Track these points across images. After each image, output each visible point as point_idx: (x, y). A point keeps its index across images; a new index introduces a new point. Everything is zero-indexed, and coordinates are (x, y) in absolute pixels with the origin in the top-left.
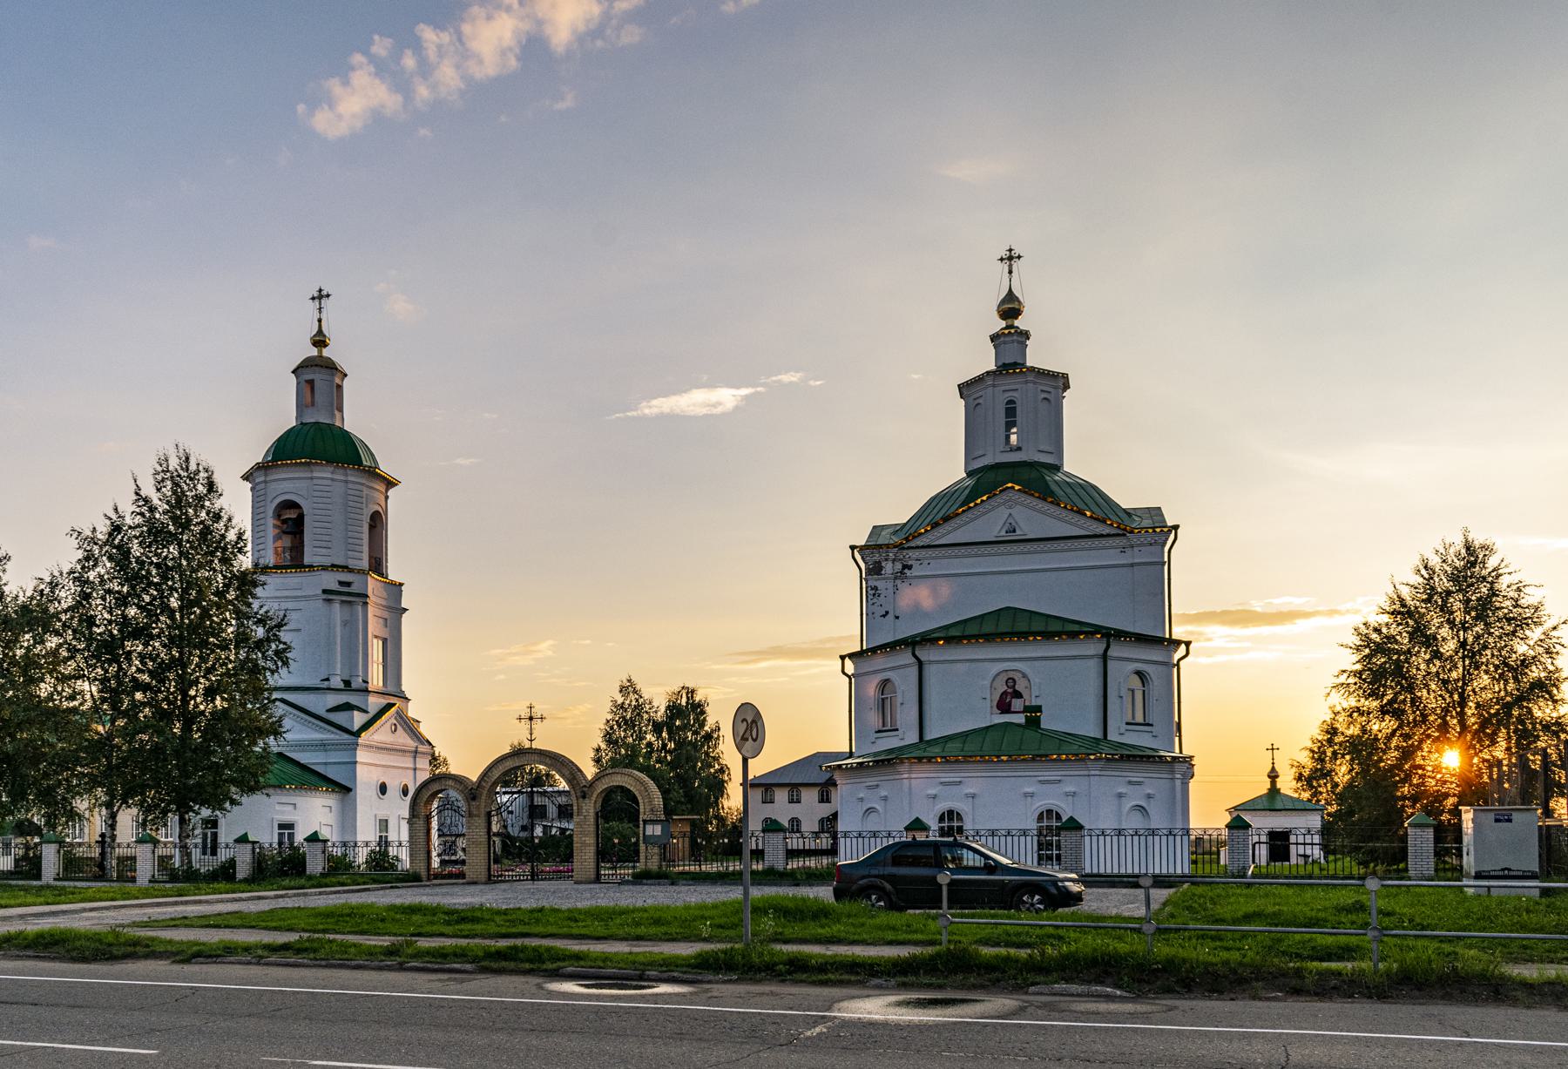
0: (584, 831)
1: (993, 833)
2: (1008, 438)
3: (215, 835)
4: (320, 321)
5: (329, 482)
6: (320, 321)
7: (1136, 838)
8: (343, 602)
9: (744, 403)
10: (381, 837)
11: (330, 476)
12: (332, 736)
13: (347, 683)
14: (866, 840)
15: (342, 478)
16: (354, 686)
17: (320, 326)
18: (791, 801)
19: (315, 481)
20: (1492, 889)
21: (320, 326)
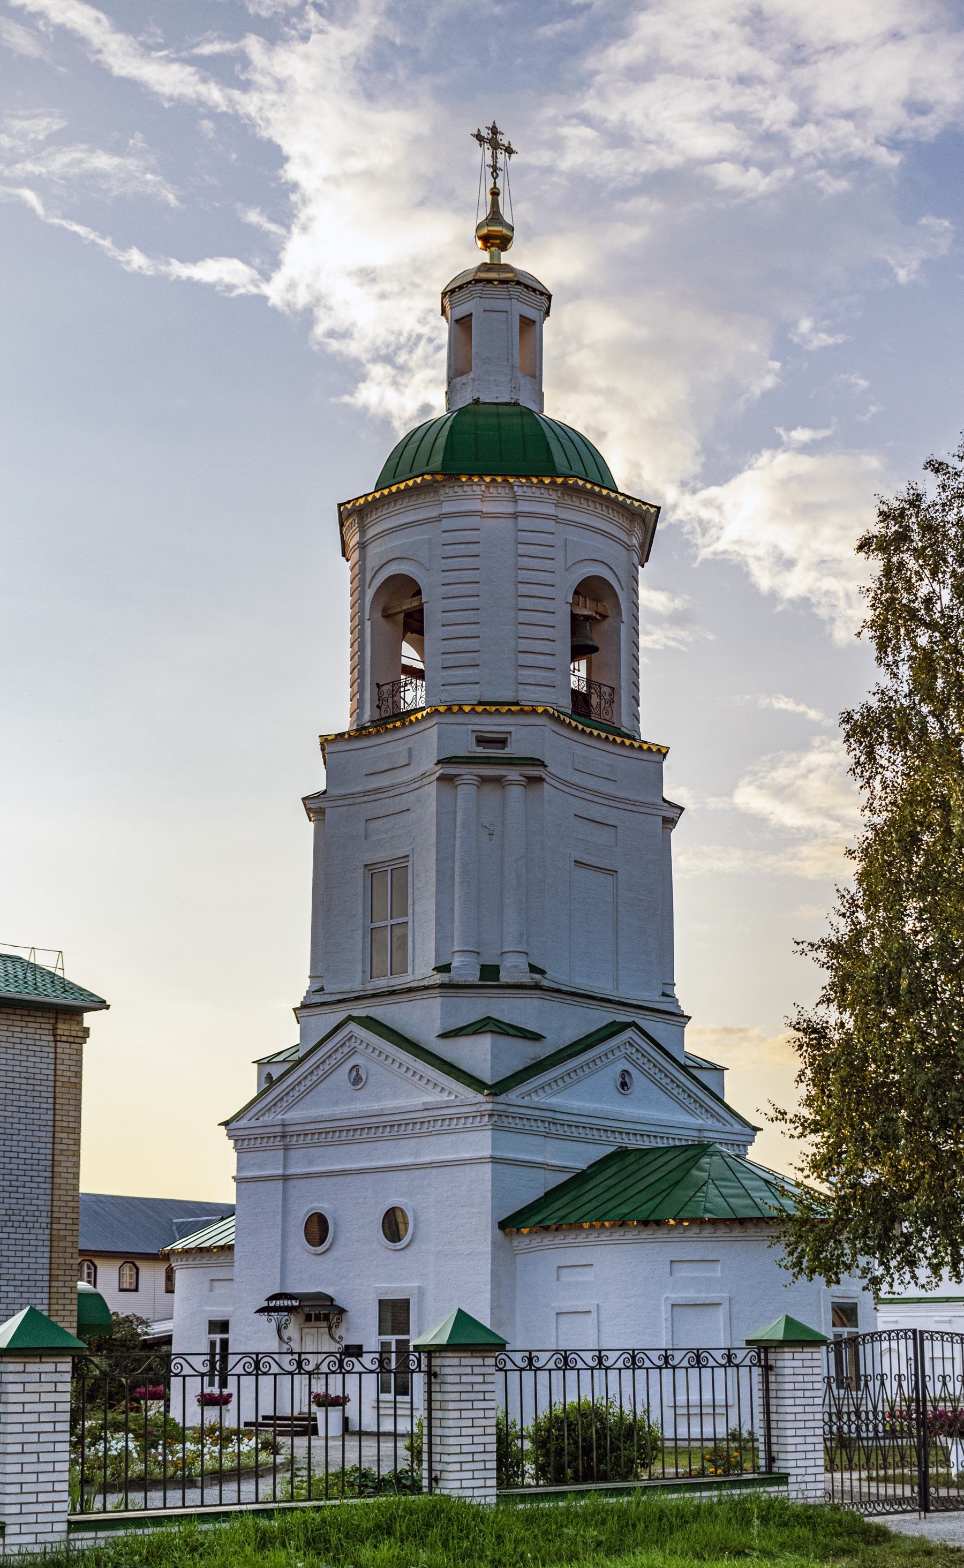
0: (218, 1337)
1: (634, 1360)
2: (428, 474)
3: (225, 1343)
4: (495, 193)
5: (550, 525)
6: (495, 193)
7: (528, 1376)
8: (484, 780)
9: (315, 348)
10: (213, 1344)
11: (550, 510)
12: (683, 1118)
13: (490, 972)
14: (680, 1373)
15: (508, 508)
16: (504, 978)
17: (495, 204)
18: (829, 1282)
19: (523, 522)
20: (162, 1506)
21: (495, 204)
